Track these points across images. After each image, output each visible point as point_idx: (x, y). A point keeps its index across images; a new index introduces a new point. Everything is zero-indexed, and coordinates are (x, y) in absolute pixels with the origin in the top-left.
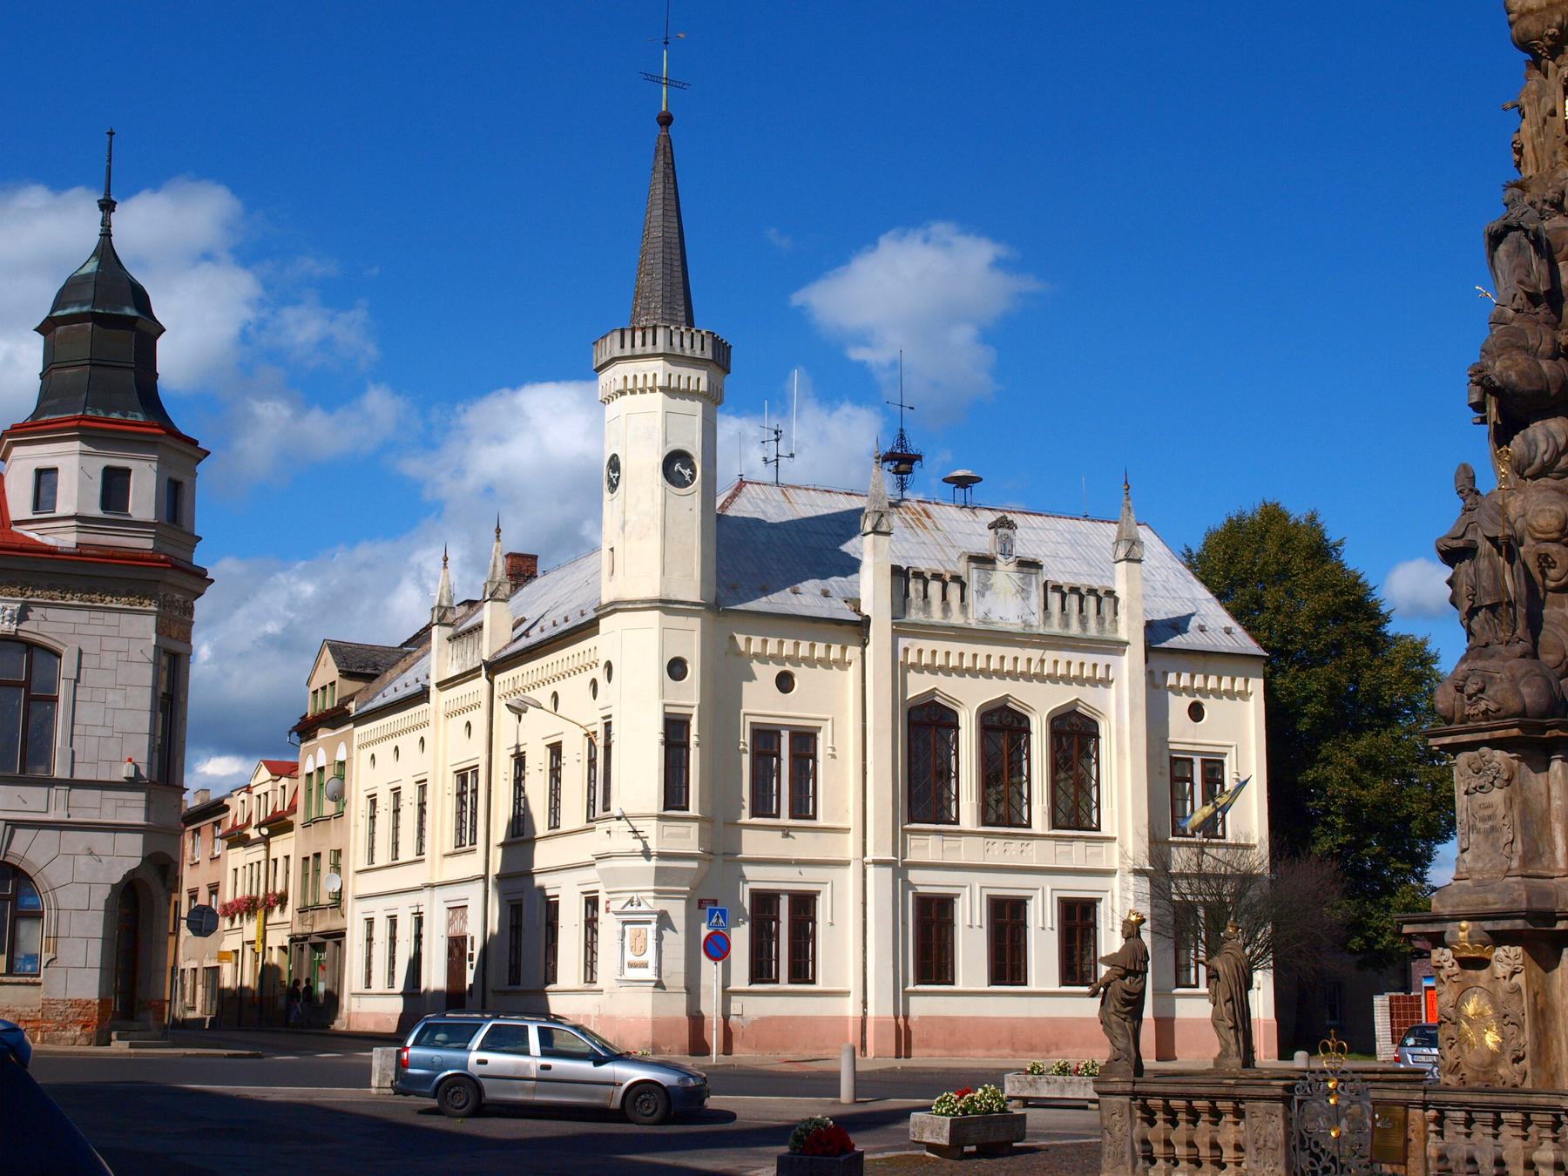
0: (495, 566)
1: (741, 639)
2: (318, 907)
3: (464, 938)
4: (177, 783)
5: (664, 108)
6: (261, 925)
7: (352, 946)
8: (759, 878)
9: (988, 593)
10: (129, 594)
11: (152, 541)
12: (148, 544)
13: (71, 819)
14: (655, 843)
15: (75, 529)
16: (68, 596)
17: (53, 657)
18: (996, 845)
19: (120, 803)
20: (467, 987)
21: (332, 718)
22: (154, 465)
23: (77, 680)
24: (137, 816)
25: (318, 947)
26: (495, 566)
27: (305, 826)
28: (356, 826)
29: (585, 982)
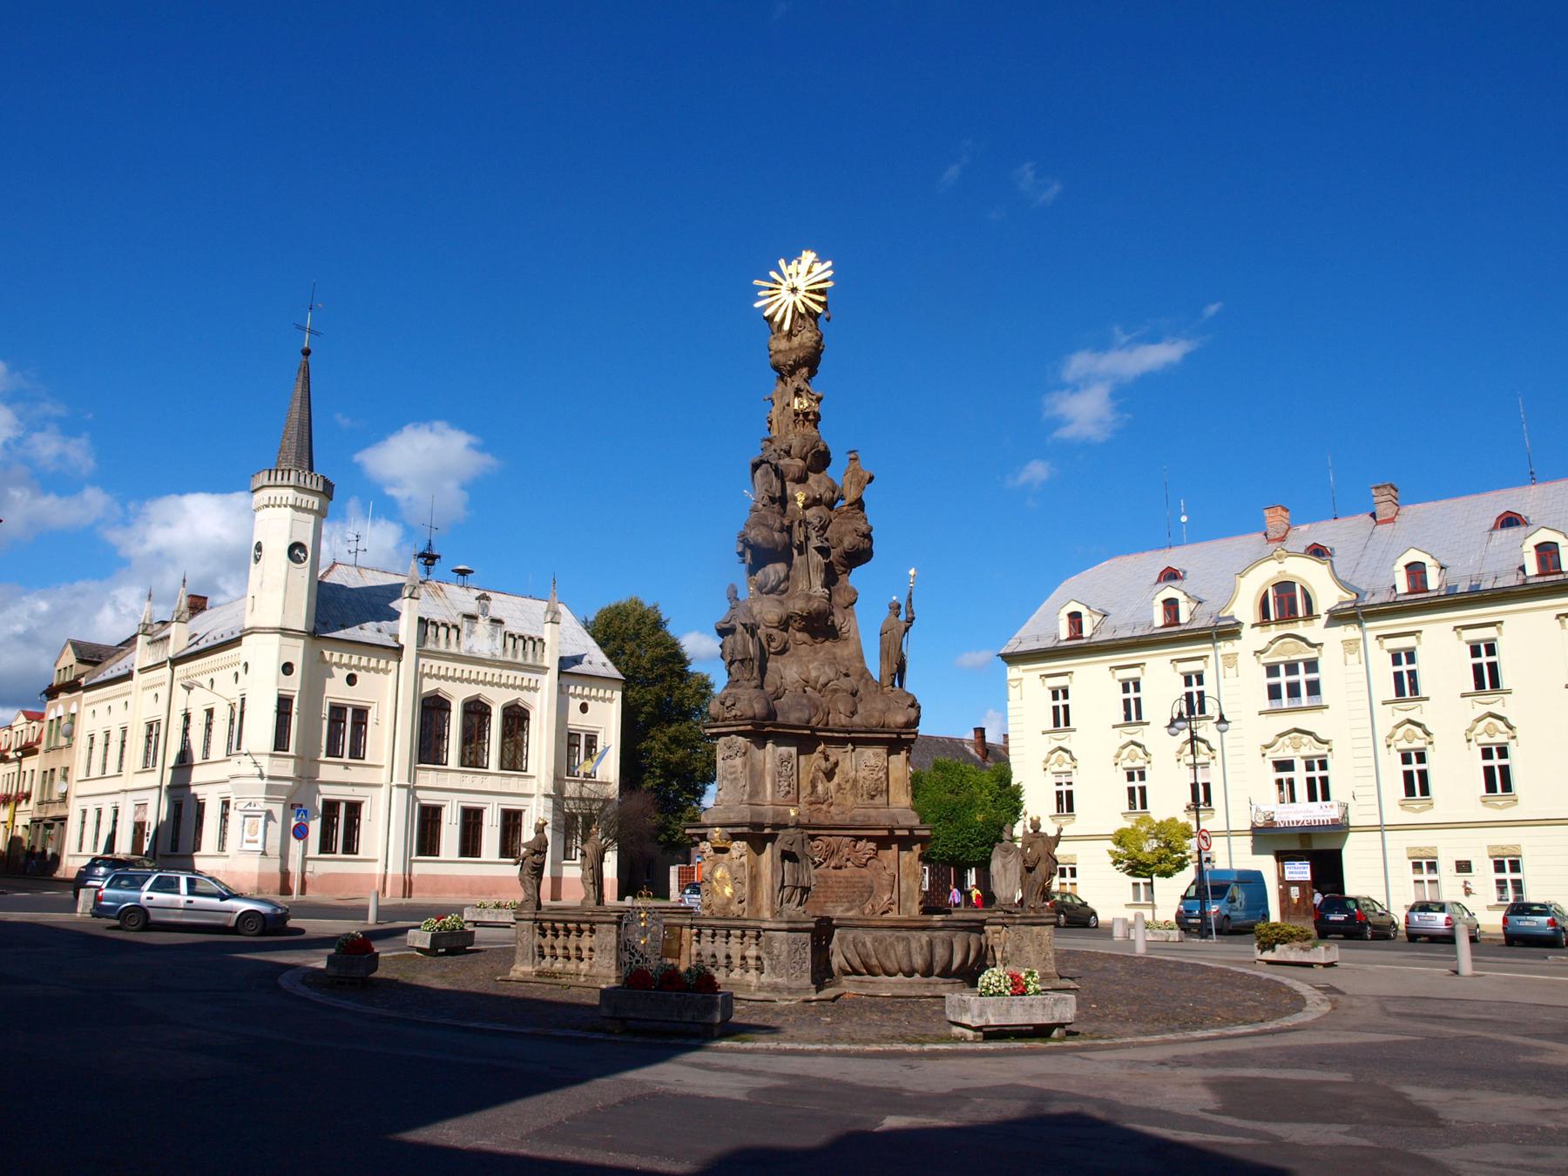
0: (181, 601)
1: (327, 654)
2: (50, 802)
6: (13, 811)
26: (181, 601)
27: (46, 752)
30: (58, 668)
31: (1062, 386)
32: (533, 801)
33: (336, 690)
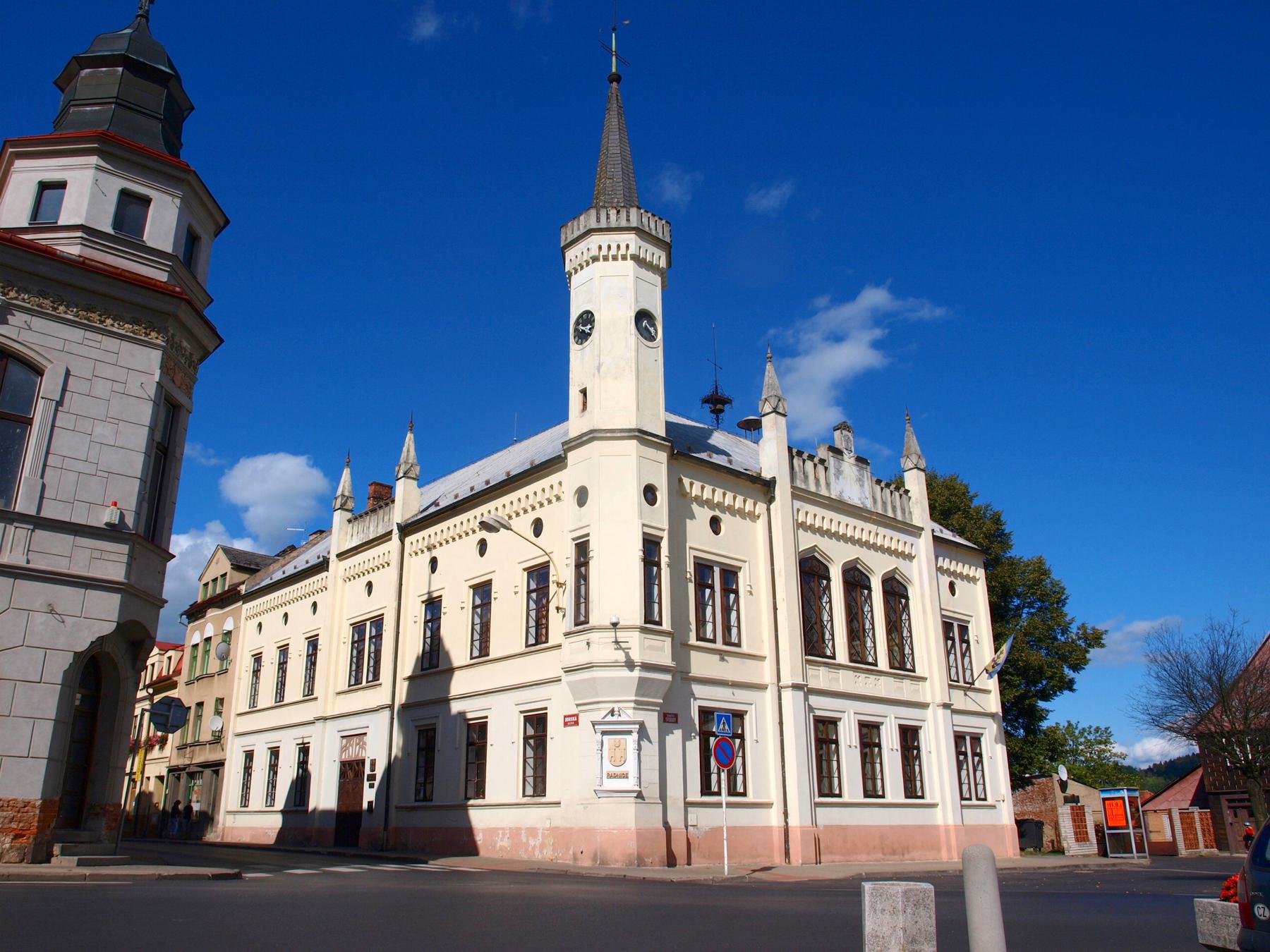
0: (408, 451)
1: (686, 481)
2: (197, 744)
3: (363, 762)
4: (163, 547)
5: (614, 70)
6: (142, 760)
7: (230, 772)
8: (705, 696)
9: (841, 477)
10: (135, 322)
11: (166, 274)
12: (162, 277)
13: (30, 566)
14: (638, 655)
15: (79, 241)
16: (62, 308)
17: (32, 376)
18: (860, 678)
19: (97, 554)
20: (365, 806)
21: (222, 599)
22: (178, 201)
23: (60, 403)
24: (117, 572)
25: (192, 775)
26: (408, 451)
27: (188, 684)
28: (240, 679)
29: (524, 795)
30: (204, 581)
31: (134, 749)
32: (929, 713)
33: (698, 537)
